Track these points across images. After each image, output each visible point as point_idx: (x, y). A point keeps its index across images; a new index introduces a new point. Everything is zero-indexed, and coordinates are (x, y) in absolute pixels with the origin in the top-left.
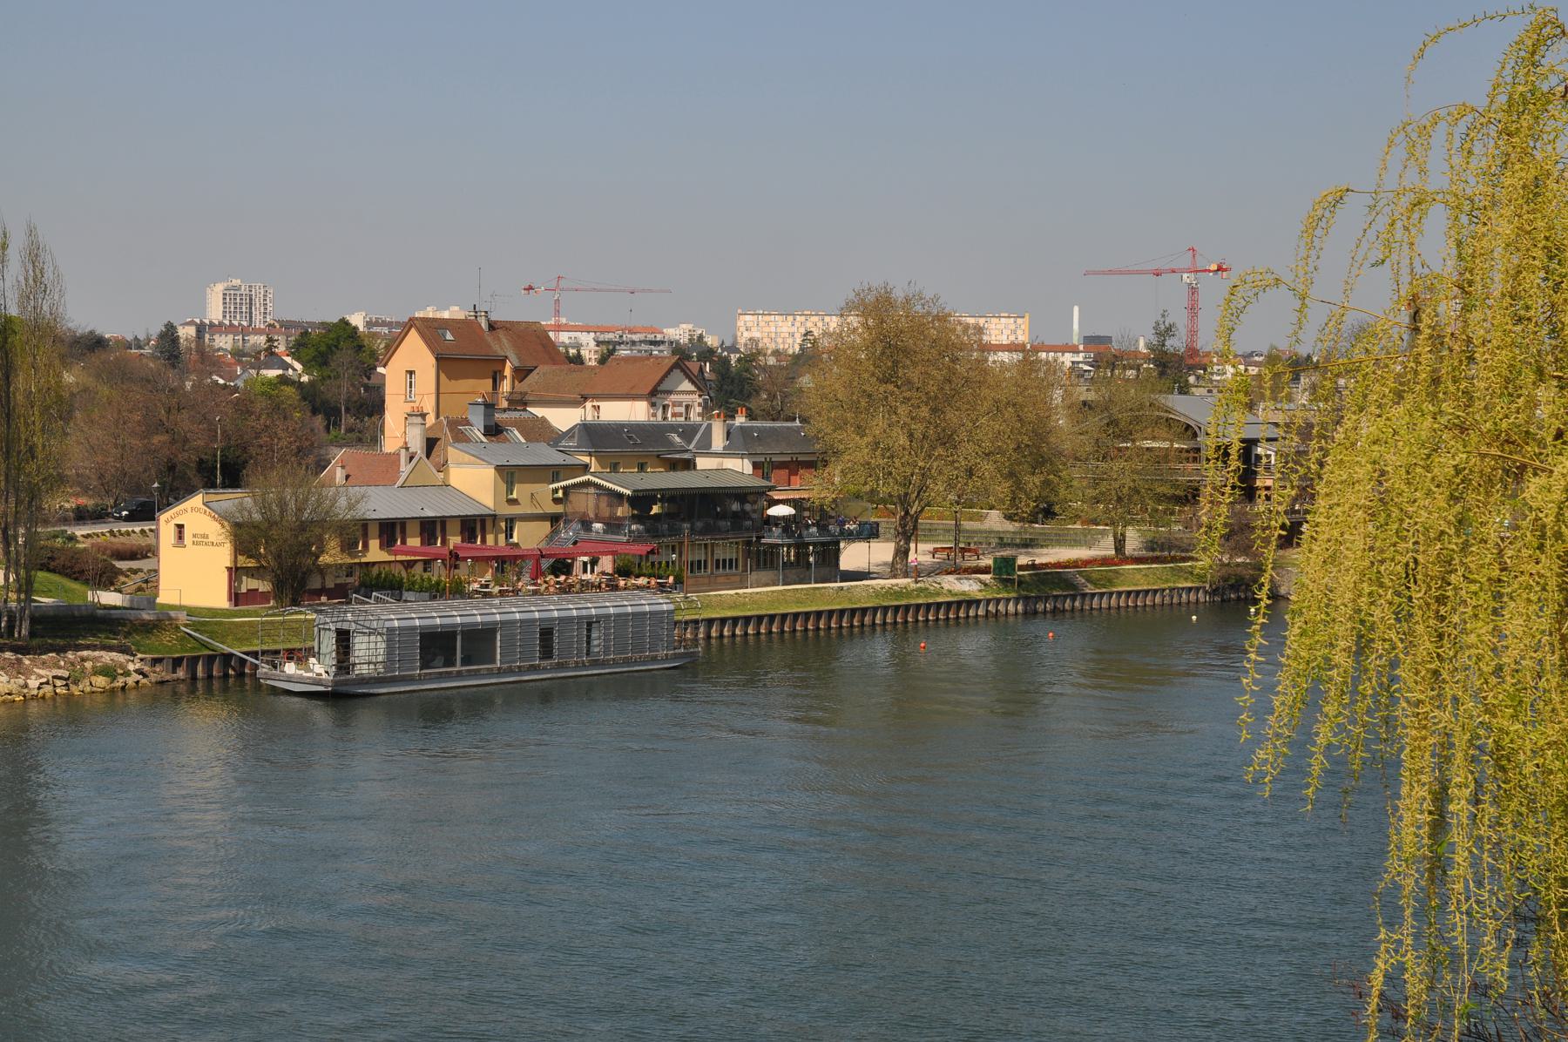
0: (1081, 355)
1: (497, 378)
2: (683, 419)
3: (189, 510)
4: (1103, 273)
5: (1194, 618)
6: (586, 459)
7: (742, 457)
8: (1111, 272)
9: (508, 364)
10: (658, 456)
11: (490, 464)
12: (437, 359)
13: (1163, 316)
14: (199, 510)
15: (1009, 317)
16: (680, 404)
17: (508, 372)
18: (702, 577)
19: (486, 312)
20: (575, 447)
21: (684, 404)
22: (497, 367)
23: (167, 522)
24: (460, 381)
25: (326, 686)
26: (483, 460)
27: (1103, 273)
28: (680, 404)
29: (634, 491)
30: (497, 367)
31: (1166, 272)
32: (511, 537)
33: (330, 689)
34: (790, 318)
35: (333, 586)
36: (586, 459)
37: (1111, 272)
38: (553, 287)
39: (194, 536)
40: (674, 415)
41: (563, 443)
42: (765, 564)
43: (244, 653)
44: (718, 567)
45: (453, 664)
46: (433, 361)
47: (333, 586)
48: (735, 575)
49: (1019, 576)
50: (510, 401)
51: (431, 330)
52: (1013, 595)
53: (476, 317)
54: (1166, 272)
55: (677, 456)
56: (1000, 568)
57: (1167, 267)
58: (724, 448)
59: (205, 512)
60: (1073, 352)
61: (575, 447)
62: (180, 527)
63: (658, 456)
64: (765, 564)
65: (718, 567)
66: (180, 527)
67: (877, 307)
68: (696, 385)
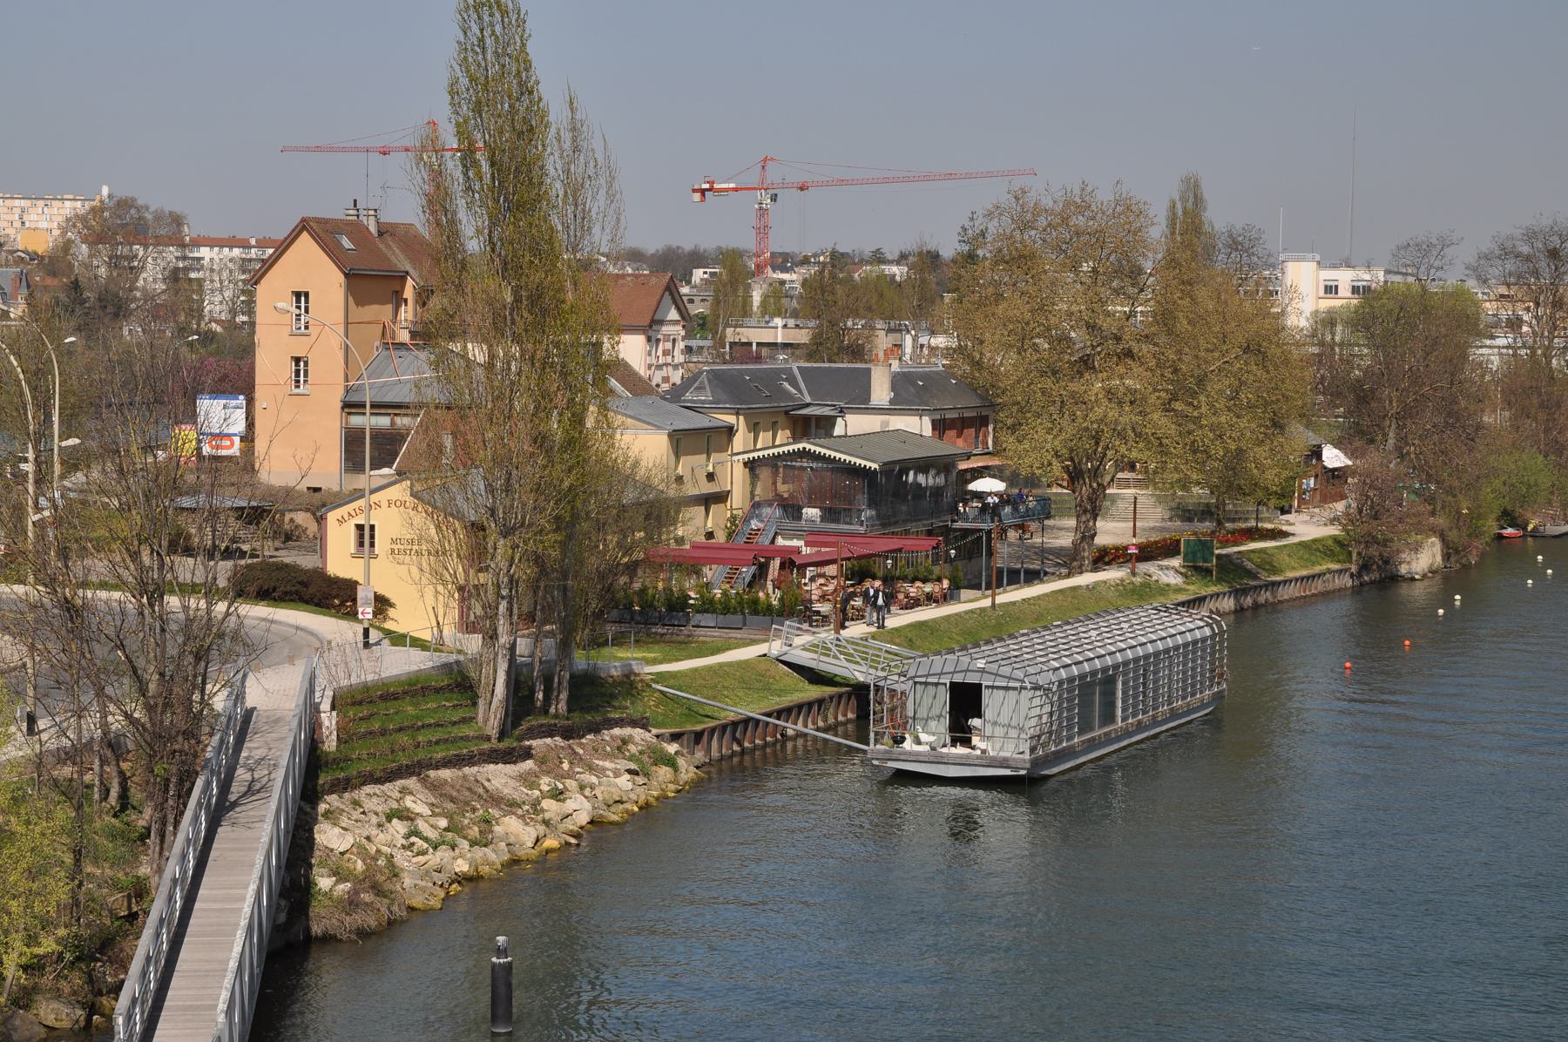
0: (253, 250)
1: (398, 300)
3: (384, 504)
4: (308, 149)
5: (1441, 611)
6: (730, 419)
7: (920, 413)
8: (318, 149)
9: (410, 282)
10: (786, 413)
11: (659, 428)
12: (346, 275)
13: (972, 219)
15: (75, 200)
17: (409, 293)
19: (376, 210)
20: (711, 403)
21: (672, 337)
22: (396, 286)
23: (341, 521)
24: (367, 307)
25: (1017, 769)
26: (649, 423)
27: (308, 149)
29: (885, 464)
30: (396, 286)
31: (397, 150)
33: (1023, 772)
34: (41, 203)
36: (730, 419)
37: (318, 149)
38: (755, 182)
41: (688, 396)
43: (769, 715)
46: (341, 278)
49: (1219, 557)
50: (414, 335)
51: (324, 232)
52: (1227, 589)
53: (358, 216)
54: (397, 150)
56: (1194, 553)
57: (398, 144)
58: (892, 402)
60: (244, 247)
61: (711, 403)
63: (786, 413)
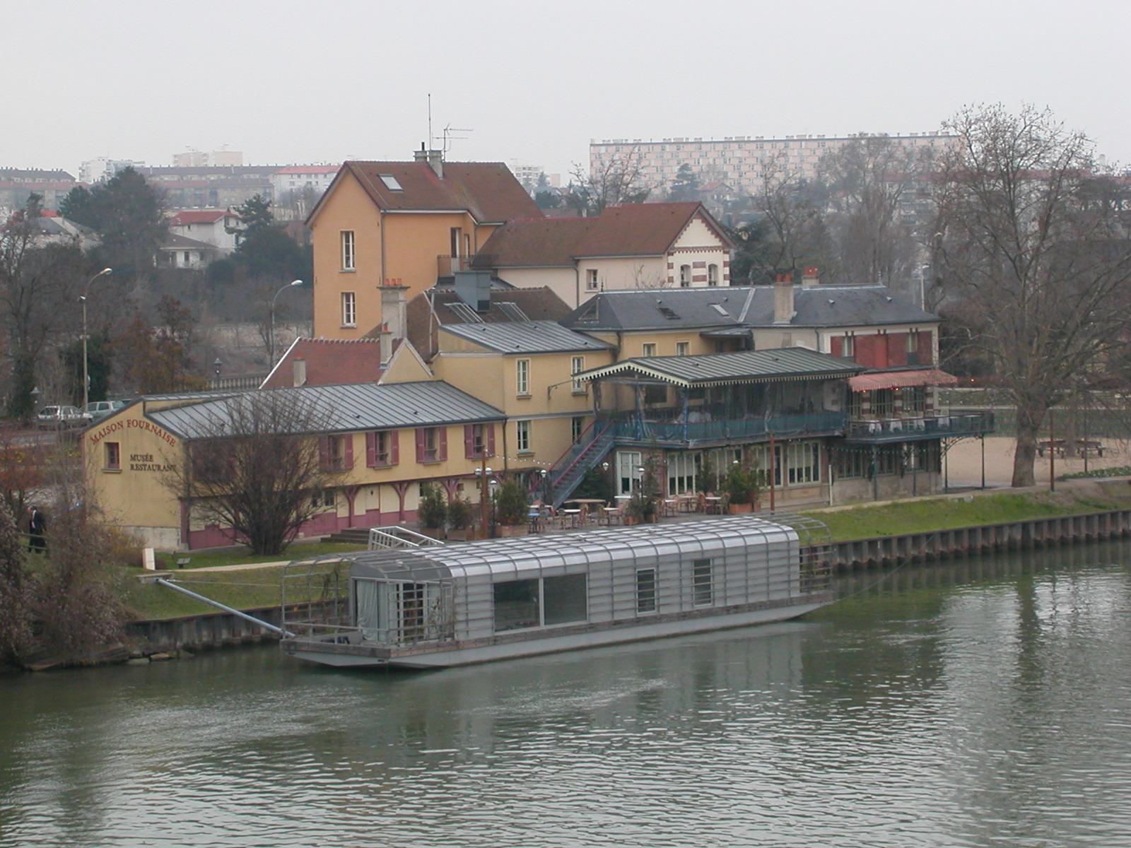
2: (705, 284)
3: (125, 424)
14: (139, 424)
16: (702, 265)
18: (813, 487)
28: (702, 265)
32: (691, 398)
35: (364, 513)
39: (134, 458)
40: (696, 279)
42: (849, 470)
44: (792, 480)
45: (537, 623)
47: (364, 513)
48: (813, 487)
55: (727, 332)
59: (148, 426)
62: (113, 448)
64: (849, 470)
65: (792, 480)
66: (113, 448)
67: (546, 287)
68: (721, 239)
